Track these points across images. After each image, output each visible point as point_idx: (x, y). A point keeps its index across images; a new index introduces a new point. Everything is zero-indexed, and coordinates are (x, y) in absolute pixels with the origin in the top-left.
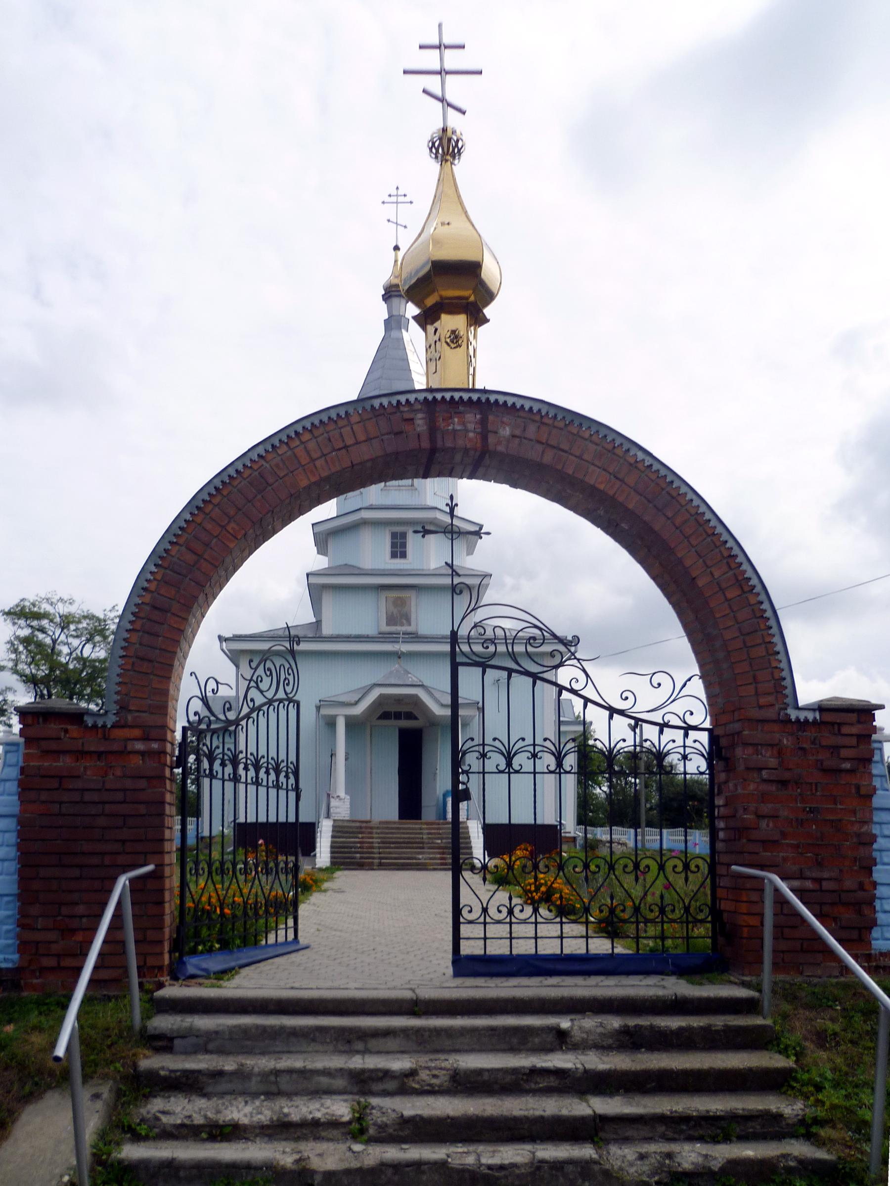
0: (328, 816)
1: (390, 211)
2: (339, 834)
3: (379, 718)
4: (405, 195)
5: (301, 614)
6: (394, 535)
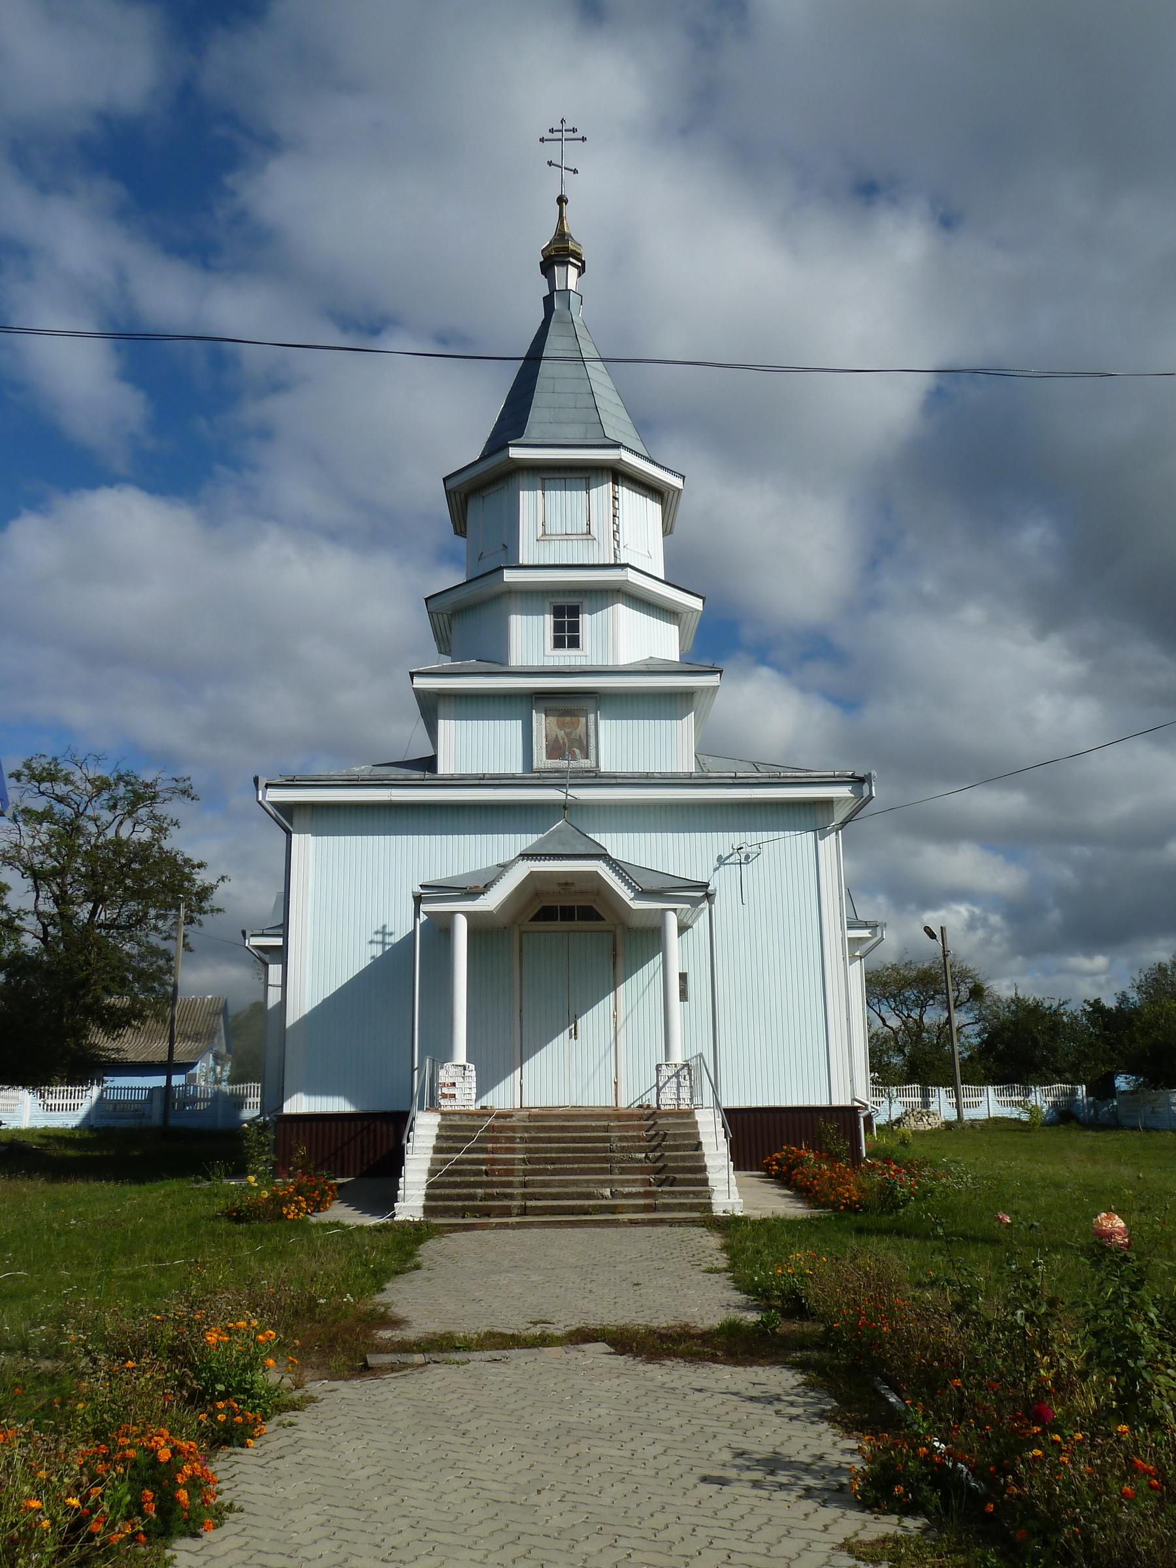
0: (433, 1106)
1: (552, 151)
2: (451, 1144)
3: (535, 919)
4: (574, 130)
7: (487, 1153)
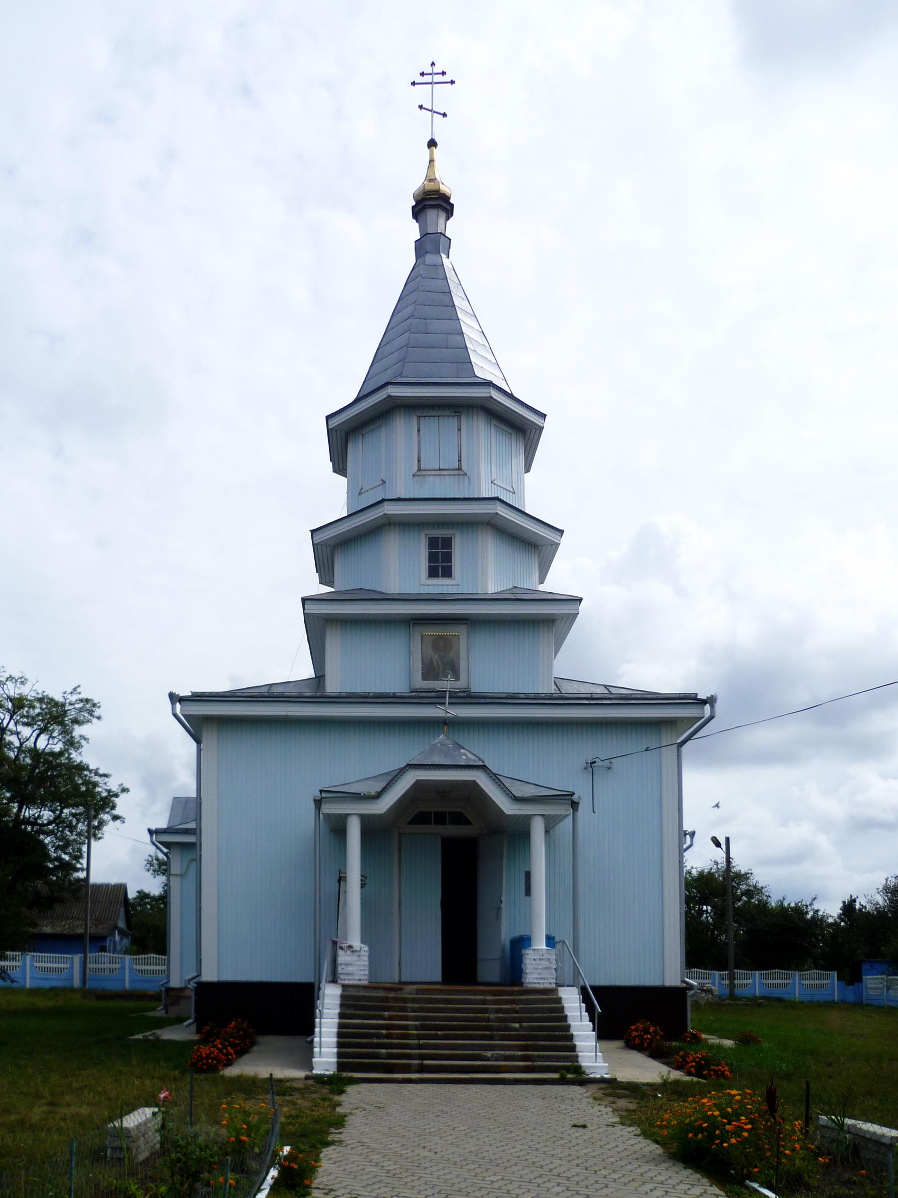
0: (334, 980)
1: (422, 94)
3: (412, 822)
4: (443, 73)
5: (298, 667)
6: (433, 543)
7: (384, 1019)
